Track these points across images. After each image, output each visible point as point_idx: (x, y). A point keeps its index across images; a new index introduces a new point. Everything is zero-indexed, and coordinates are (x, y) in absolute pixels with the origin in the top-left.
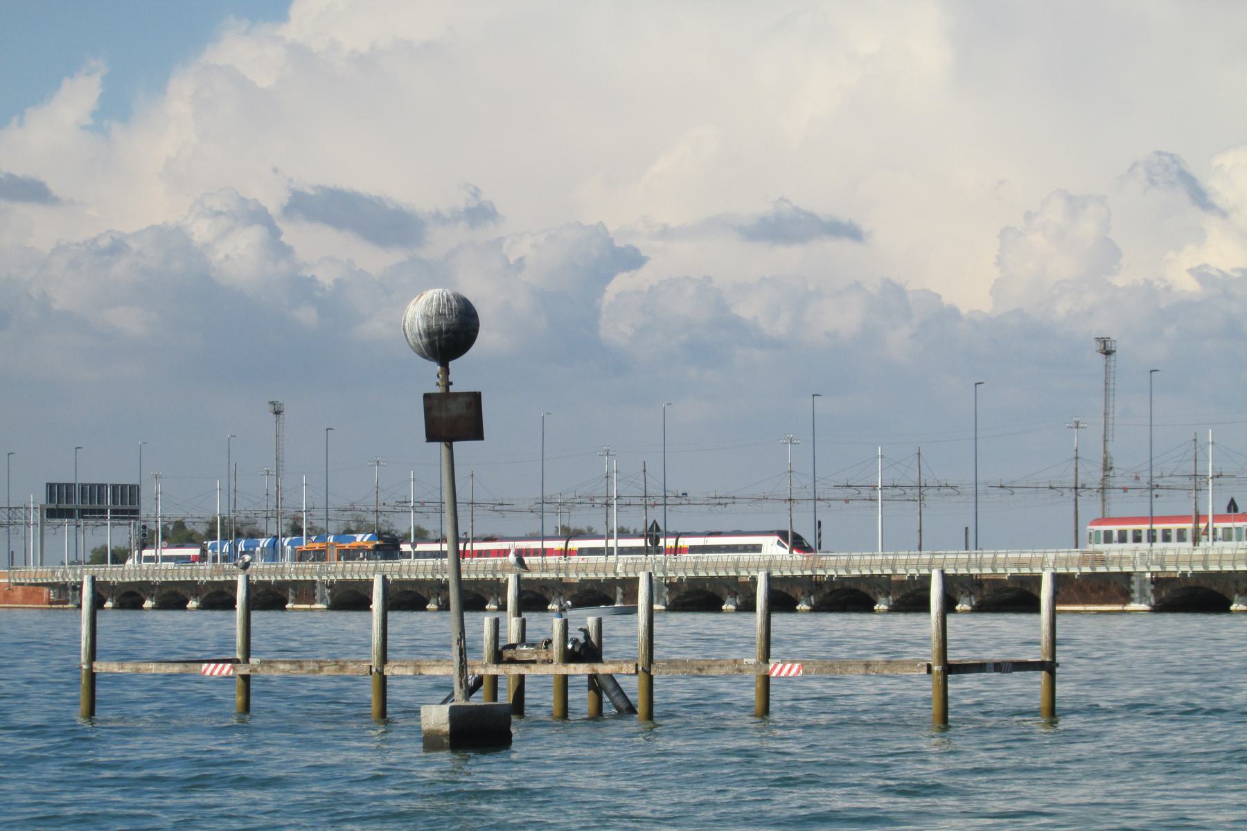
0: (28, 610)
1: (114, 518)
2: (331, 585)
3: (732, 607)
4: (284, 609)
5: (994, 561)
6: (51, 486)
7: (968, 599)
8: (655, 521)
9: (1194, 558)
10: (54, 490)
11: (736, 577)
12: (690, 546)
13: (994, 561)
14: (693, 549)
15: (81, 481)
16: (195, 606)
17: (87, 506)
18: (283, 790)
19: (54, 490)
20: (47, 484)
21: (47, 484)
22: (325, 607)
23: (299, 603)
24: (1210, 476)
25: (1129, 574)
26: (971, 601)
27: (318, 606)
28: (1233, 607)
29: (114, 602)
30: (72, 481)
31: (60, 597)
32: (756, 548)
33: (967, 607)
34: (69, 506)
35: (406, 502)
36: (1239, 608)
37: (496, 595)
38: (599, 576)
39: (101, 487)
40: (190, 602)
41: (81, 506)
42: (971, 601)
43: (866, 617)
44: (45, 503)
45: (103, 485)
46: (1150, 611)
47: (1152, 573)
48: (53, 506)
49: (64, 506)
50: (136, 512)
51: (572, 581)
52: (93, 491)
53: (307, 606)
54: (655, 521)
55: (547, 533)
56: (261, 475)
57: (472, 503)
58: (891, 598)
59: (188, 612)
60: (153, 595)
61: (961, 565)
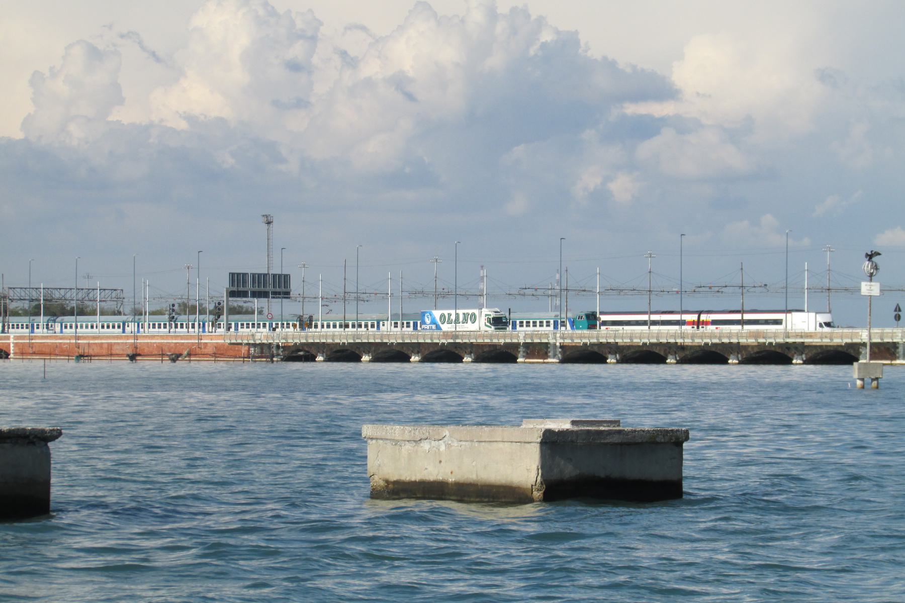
0: (118, 361)
1: (274, 298)
2: (562, 347)
3: (614, 361)
4: (409, 362)
5: (432, 335)
6: (232, 275)
7: (614, 356)
8: (898, 304)
9: (575, 335)
10: (237, 278)
11: (739, 343)
12: (712, 320)
13: (432, 335)
14: (714, 322)
15: (271, 272)
16: (368, 360)
17: (256, 289)
18: (742, 483)
19: (237, 278)
20: (230, 273)
21: (230, 273)
22: (558, 361)
23: (529, 358)
24: (806, 287)
25: (547, 344)
26: (676, 358)
27: (550, 360)
28: (729, 361)
29: (325, 357)
30: (280, 273)
31: (262, 352)
32: (777, 322)
33: (470, 359)
34: (245, 289)
35: (315, 298)
36: (798, 362)
37: (736, 353)
38: (500, 341)
39: (244, 275)
40: (364, 357)
41: (273, 290)
42: (676, 358)
43: (662, 366)
44: (228, 287)
45: (246, 274)
46: (559, 362)
47: (282, 343)
48: (235, 289)
49: (241, 289)
50: (288, 293)
51: (290, 345)
52: (259, 278)
53: (541, 361)
54: (898, 304)
55: (746, 308)
56: (824, 251)
57: (456, 295)
58: (804, 356)
59: (317, 363)
60: (323, 352)
61: (610, 337)
